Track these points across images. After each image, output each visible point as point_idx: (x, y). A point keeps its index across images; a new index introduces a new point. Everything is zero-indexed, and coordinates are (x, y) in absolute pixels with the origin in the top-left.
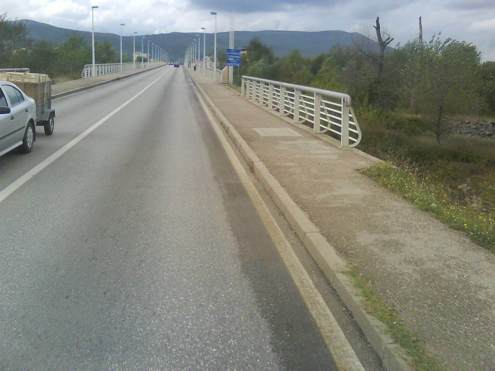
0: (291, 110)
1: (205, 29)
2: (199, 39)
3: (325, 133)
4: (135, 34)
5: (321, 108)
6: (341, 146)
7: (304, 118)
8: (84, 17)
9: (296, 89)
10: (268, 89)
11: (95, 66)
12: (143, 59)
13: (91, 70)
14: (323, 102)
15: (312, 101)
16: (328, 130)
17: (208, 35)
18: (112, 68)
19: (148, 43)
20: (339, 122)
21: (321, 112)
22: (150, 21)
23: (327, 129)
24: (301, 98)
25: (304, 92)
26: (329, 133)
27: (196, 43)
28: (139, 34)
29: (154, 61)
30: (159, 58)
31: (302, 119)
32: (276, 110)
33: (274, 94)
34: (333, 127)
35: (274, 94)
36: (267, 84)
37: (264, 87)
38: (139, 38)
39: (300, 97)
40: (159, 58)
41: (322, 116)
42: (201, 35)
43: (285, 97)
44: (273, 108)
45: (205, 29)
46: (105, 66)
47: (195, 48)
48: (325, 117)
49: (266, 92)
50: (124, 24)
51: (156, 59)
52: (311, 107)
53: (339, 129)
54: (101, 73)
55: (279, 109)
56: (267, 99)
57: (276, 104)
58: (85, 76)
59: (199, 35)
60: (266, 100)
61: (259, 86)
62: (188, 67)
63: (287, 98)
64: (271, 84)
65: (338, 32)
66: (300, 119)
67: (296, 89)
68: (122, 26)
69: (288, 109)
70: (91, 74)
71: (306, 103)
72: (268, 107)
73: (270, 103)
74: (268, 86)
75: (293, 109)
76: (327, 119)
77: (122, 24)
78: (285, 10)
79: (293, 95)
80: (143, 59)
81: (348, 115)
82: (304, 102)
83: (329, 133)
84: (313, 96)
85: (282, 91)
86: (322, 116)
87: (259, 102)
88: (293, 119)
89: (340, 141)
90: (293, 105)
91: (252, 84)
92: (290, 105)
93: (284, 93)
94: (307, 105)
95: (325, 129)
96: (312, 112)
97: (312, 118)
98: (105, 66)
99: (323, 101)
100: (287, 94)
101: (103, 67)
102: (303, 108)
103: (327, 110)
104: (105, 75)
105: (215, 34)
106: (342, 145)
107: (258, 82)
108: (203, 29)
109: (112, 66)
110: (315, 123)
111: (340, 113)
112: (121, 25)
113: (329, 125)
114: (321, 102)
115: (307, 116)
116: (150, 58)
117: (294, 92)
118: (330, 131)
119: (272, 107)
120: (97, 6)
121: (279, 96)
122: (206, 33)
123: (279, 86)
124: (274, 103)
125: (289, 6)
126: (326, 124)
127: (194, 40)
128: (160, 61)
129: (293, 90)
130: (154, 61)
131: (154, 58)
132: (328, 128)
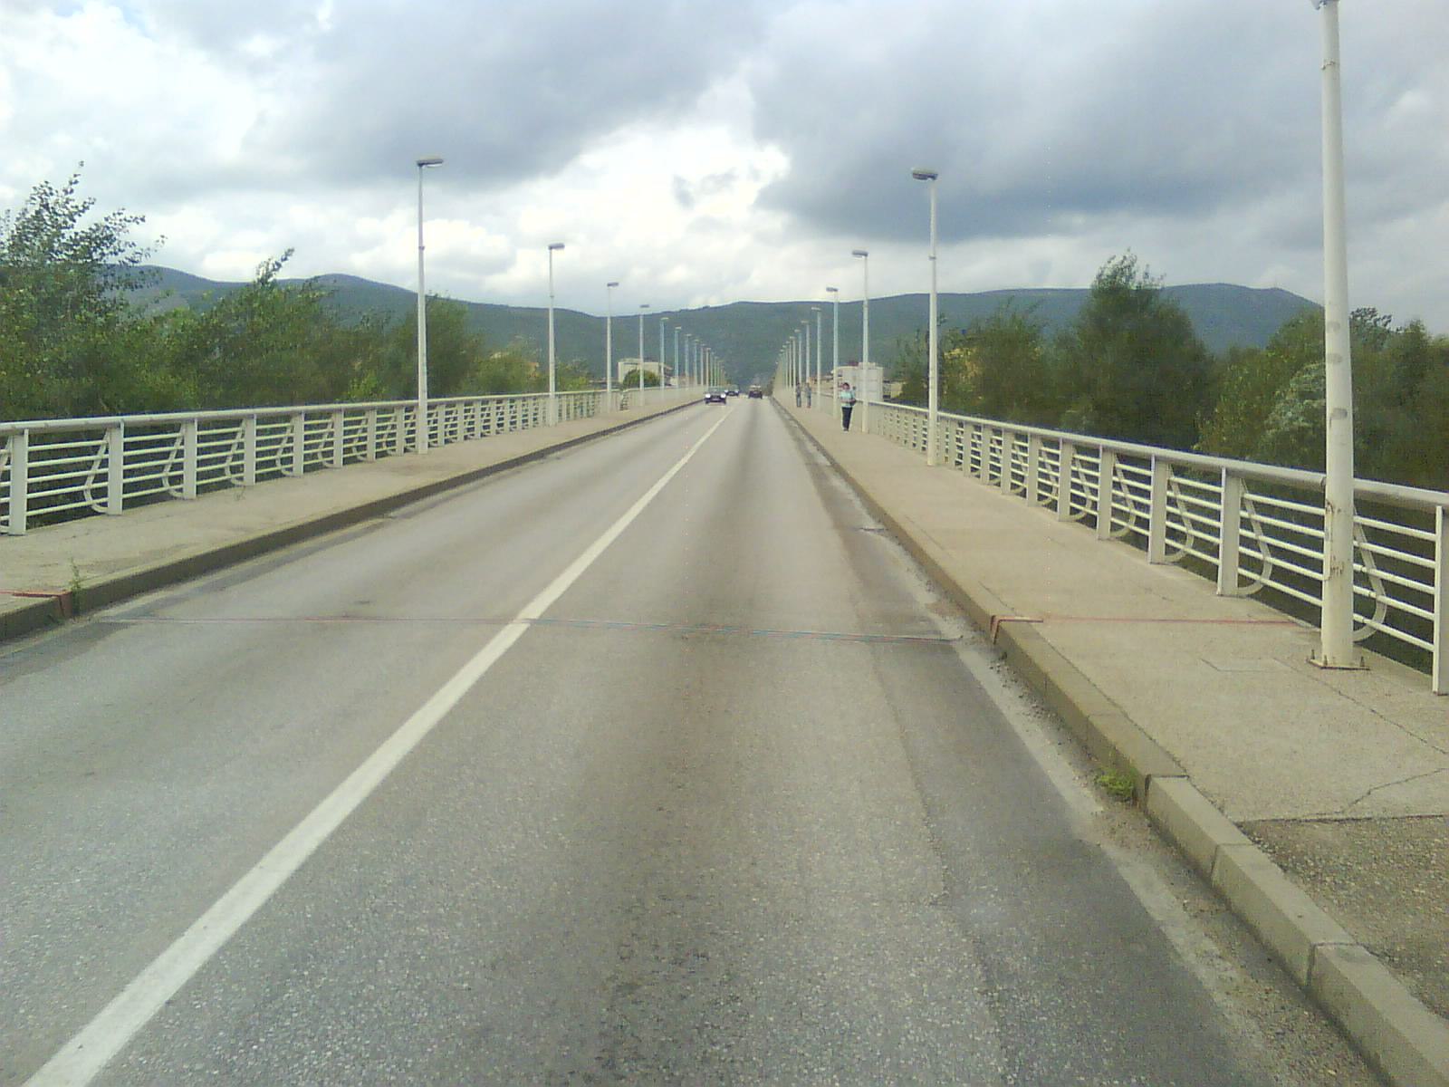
0: (1089, 504)
1: (835, 290)
2: (819, 319)
3: (1364, 641)
4: (644, 309)
5: (1242, 518)
6: (1431, 687)
7: (1046, 494)
8: (501, 265)
9: (1104, 450)
10: (1024, 449)
11: (556, 395)
12: (1336, 343)
13: (544, 408)
14: (1249, 500)
15: (1215, 497)
16: (1266, 586)
17: (845, 307)
18: (565, 404)
19: (662, 326)
20: (1215, 531)
21: (1013, 461)
22: (678, 274)
23: (1184, 552)
24: (1016, 447)
25: (1180, 469)
26: (1377, 643)
27: (794, 343)
28: (656, 308)
29: (682, 384)
30: (699, 374)
31: (1078, 511)
32: (1081, 521)
33: (1015, 456)
34: (1200, 544)
35: (1015, 456)
36: (1022, 436)
37: (1040, 452)
38: (652, 320)
39: (1013, 445)
40: (699, 374)
41: (1245, 541)
42: (826, 307)
43: (1073, 471)
44: (1039, 500)
45: (835, 290)
46: (500, 401)
47: (797, 351)
48: (1079, 487)
49: (1082, 476)
50: (616, 284)
51: (687, 379)
52: (1142, 496)
53: (1214, 551)
54: (535, 419)
55: (1056, 501)
56: (999, 468)
57: (1049, 489)
58: (490, 430)
59: (818, 309)
60: (978, 462)
61: (999, 443)
62: (799, 405)
63: (1077, 472)
64: (1106, 449)
65: (1221, 287)
66: (1244, 581)
67: (1157, 459)
68: (611, 287)
69: (1082, 501)
70: (544, 417)
71: (1086, 475)
72: (1354, 629)
73: (1030, 485)
74: (980, 431)
75: (1057, 489)
76: (1083, 491)
77: (611, 282)
78: (1066, 231)
79: (1095, 467)
80: (1336, 343)
81: (1238, 513)
82: (1256, 521)
83: (1189, 563)
84: (1217, 482)
85: (1065, 453)
86: (1245, 541)
87: (999, 485)
88: (1056, 510)
89: (1214, 583)
90: (1094, 492)
91: (962, 432)
92: (1374, 586)
93: (1011, 446)
94: (1134, 490)
95: (1122, 527)
96: (1146, 508)
97: (1144, 523)
98: (500, 401)
99: (1043, 448)
100: (1120, 473)
101: (519, 403)
102: (1252, 540)
103: (1129, 486)
104: (570, 423)
105: (866, 303)
106: (1435, 688)
107: (978, 427)
108: (829, 290)
109: (564, 398)
110: (1152, 534)
111: (1431, 566)
112: (609, 285)
113: (1268, 571)
114: (1242, 499)
115: (1190, 541)
116: (669, 374)
117: (1027, 442)
118: (1193, 556)
119: (970, 469)
120: (558, 242)
121: (1025, 459)
122: (840, 304)
123: (1098, 450)
124: (1015, 476)
125: (1079, 220)
126: (1255, 565)
127: (796, 331)
128: (699, 383)
129: (1094, 451)
130: (682, 384)
131: (682, 374)
132: (1264, 577)
